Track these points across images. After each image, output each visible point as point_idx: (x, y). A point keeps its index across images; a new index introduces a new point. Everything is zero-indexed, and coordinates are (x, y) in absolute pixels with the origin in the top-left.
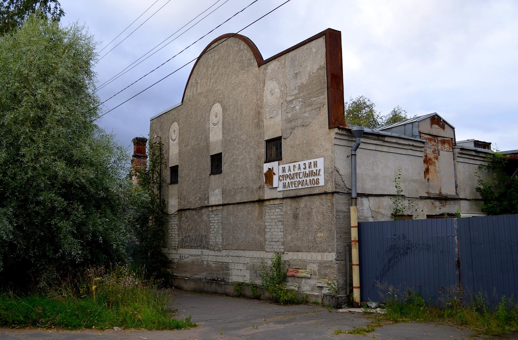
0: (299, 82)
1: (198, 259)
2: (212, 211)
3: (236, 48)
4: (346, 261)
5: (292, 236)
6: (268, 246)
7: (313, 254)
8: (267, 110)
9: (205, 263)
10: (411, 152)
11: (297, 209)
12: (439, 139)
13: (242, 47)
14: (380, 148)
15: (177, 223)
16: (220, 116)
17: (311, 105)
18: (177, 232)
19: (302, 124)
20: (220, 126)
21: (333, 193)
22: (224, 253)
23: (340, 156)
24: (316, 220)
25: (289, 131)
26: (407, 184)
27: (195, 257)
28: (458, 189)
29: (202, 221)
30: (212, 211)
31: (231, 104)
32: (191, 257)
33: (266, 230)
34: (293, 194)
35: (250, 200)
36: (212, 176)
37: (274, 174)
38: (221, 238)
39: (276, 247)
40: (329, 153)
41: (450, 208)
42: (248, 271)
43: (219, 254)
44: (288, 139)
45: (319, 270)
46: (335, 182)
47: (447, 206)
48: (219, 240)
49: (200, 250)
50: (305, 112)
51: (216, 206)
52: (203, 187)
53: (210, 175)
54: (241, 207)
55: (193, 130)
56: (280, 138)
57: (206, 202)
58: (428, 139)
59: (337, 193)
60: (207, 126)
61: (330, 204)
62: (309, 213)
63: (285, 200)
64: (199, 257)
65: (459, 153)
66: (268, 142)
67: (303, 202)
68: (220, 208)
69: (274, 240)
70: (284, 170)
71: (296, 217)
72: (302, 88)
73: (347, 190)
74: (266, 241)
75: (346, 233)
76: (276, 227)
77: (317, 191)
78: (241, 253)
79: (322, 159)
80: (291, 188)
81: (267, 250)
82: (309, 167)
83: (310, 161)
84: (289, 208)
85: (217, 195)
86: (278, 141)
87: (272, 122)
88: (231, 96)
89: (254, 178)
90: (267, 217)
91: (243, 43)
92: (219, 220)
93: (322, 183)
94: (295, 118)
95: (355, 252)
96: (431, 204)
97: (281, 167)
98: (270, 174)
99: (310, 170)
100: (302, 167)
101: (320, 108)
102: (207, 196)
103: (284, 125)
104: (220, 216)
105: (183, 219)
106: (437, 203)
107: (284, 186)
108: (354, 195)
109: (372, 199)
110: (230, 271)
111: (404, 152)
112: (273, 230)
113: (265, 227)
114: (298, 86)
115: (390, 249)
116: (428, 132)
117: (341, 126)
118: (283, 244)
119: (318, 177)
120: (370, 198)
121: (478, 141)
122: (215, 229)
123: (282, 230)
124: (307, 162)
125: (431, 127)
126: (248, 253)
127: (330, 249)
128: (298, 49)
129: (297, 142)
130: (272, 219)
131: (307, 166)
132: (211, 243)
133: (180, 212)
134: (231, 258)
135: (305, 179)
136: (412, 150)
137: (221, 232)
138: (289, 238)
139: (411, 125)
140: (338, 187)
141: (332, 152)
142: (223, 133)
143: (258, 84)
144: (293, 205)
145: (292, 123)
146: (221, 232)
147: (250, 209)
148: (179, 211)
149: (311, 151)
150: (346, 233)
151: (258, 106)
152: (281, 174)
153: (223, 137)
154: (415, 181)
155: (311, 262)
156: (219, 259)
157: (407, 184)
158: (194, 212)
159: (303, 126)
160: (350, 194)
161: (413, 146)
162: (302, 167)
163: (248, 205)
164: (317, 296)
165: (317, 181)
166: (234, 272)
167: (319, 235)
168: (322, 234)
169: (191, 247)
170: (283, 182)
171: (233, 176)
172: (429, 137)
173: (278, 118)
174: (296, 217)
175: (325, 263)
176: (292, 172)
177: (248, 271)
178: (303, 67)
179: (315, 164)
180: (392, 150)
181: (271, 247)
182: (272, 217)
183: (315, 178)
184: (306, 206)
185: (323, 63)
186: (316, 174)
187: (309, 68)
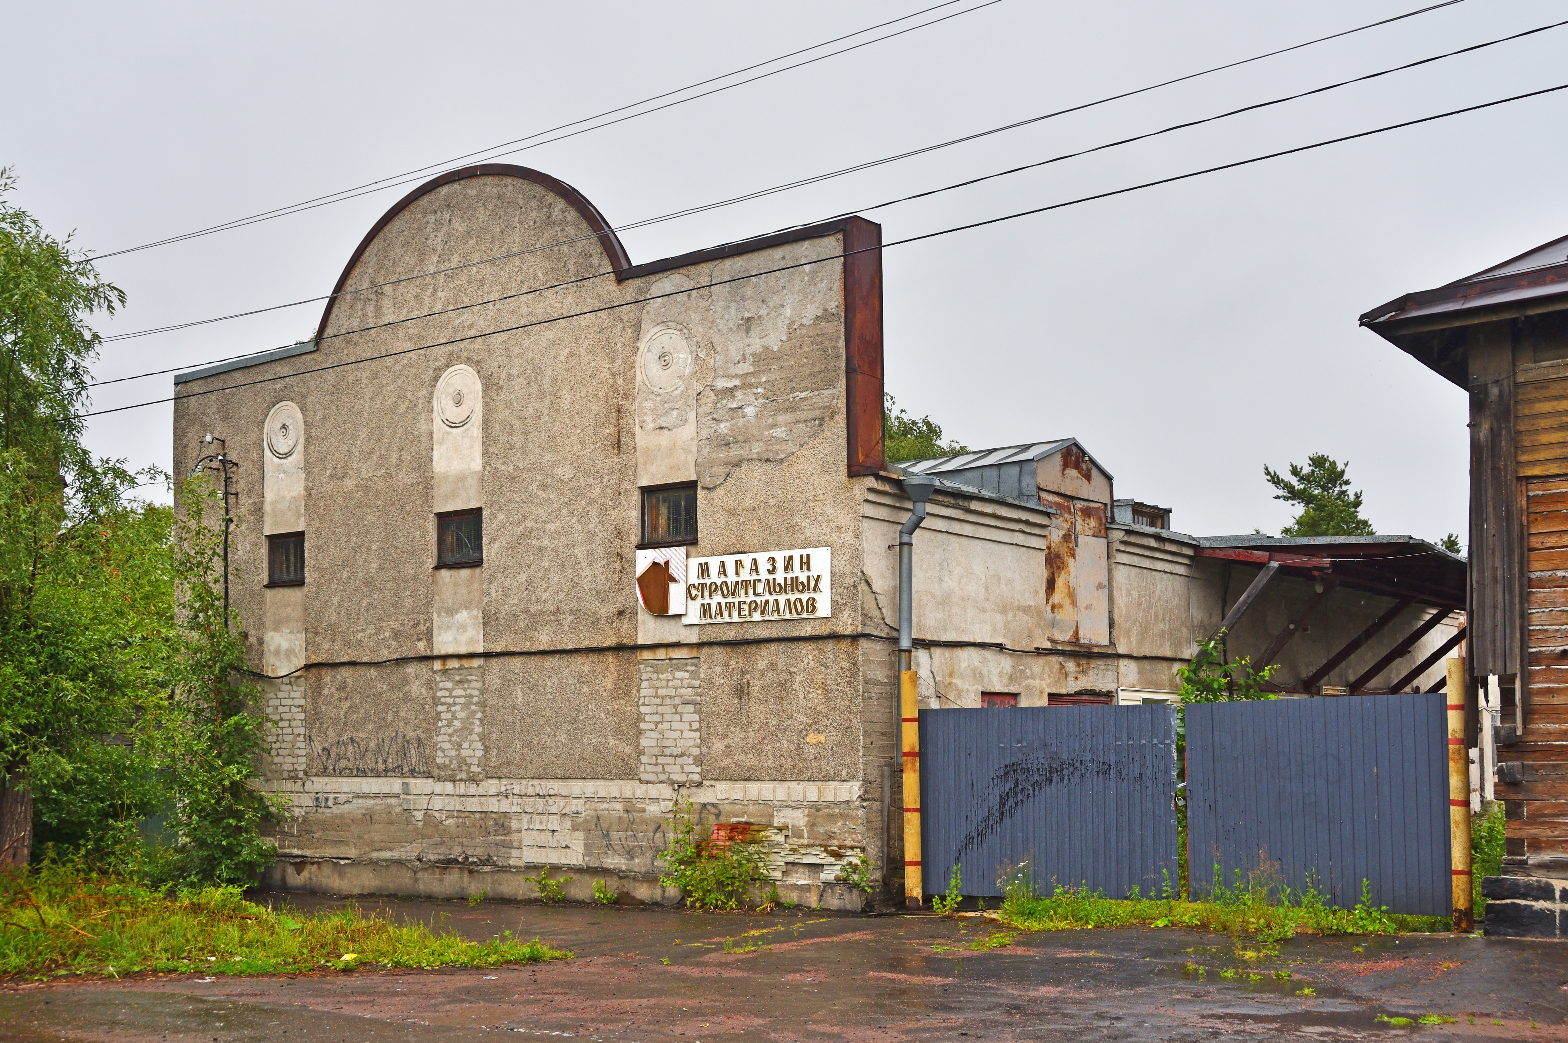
0: (756, 344)
1: (390, 806)
2: (445, 672)
3: (534, 214)
4: (882, 801)
5: (727, 741)
6: (649, 768)
7: (793, 785)
8: (649, 404)
9: (419, 815)
10: (1019, 538)
11: (743, 673)
12: (1079, 505)
13: (556, 213)
14: (956, 527)
15: (302, 702)
16: (475, 403)
17: (792, 408)
18: (302, 731)
19: (765, 457)
20: (475, 430)
21: (855, 638)
22: (492, 786)
23: (875, 542)
24: (803, 703)
25: (720, 470)
26: (1010, 616)
27: (379, 801)
28: (1115, 633)
29: (407, 698)
30: (445, 672)
31: (514, 372)
32: (360, 801)
33: (642, 726)
34: (731, 634)
35: (586, 644)
36: (444, 573)
37: (674, 580)
38: (479, 745)
39: (677, 768)
40: (849, 537)
41: (1098, 678)
42: (580, 835)
43: (472, 789)
44: (720, 492)
45: (812, 825)
46: (863, 609)
47: (1091, 673)
48: (473, 751)
49: (400, 781)
50: (774, 426)
51: (460, 657)
52: (408, 602)
53: (437, 568)
54: (550, 662)
55: (363, 433)
56: (692, 485)
57: (421, 645)
58: (1058, 505)
59: (867, 636)
60: (423, 427)
61: (845, 664)
62: (783, 685)
63: (705, 651)
64: (393, 801)
65: (1122, 542)
66: (650, 493)
67: (762, 658)
68: (476, 663)
69: (668, 751)
70: (704, 570)
71: (742, 692)
72: (763, 359)
73: (887, 630)
74: (641, 753)
75: (883, 734)
76: (678, 717)
77: (807, 630)
78: (555, 786)
79: (826, 552)
80: (727, 619)
81: (644, 777)
82: (786, 569)
83: (788, 553)
84: (718, 670)
85: (463, 627)
86: (690, 492)
87: (664, 440)
88: (516, 351)
89: (599, 587)
90: (643, 692)
91: (560, 204)
92: (471, 696)
93: (824, 609)
94: (740, 438)
95: (911, 780)
96: (1058, 666)
97: (694, 562)
98: (657, 580)
99: (789, 576)
100: (764, 566)
101: (822, 419)
102: (423, 628)
103: (705, 452)
104: (478, 685)
105: (325, 691)
106: (1071, 666)
107: (705, 611)
108: (905, 643)
109: (937, 652)
110: (515, 837)
111: (1005, 537)
112: (666, 726)
113: (640, 718)
114: (754, 355)
115: (1006, 773)
116: (1056, 489)
117: (882, 473)
118: (699, 761)
119: (812, 595)
120: (933, 649)
121: (1142, 504)
122: (457, 723)
123: (696, 726)
124: (780, 556)
125: (1063, 474)
126: (576, 787)
127: (844, 773)
128: (756, 254)
129: (748, 502)
130: (663, 697)
131: (780, 565)
132: (439, 761)
133: (314, 671)
134: (516, 800)
135: (771, 599)
136: (1023, 532)
137: (478, 730)
138: (719, 746)
139: (1016, 470)
140: (867, 621)
141: (857, 536)
142: (486, 453)
143: (618, 330)
144: (733, 662)
145: (731, 451)
146: (478, 730)
147: (586, 668)
148: (308, 667)
149: (792, 528)
150: (883, 734)
151: (616, 391)
152: (694, 579)
153: (486, 464)
154: (1026, 610)
155: (784, 805)
156: (473, 805)
157: (1010, 616)
158: (373, 673)
159: (768, 460)
160: (896, 641)
161: (1027, 523)
162: (764, 566)
163: (579, 659)
164: (806, 888)
165: (811, 606)
166: (528, 839)
167: (812, 738)
168: (822, 738)
169: (363, 773)
170: (699, 601)
171: (523, 577)
172: (1057, 499)
173: (688, 431)
174: (742, 692)
175: (828, 807)
176: (732, 578)
177: (580, 835)
178: (771, 304)
179: (805, 563)
180: (982, 532)
181: (659, 769)
182: (661, 692)
183: (805, 597)
184: (773, 666)
185: (833, 304)
186: (805, 587)
187: (788, 312)
